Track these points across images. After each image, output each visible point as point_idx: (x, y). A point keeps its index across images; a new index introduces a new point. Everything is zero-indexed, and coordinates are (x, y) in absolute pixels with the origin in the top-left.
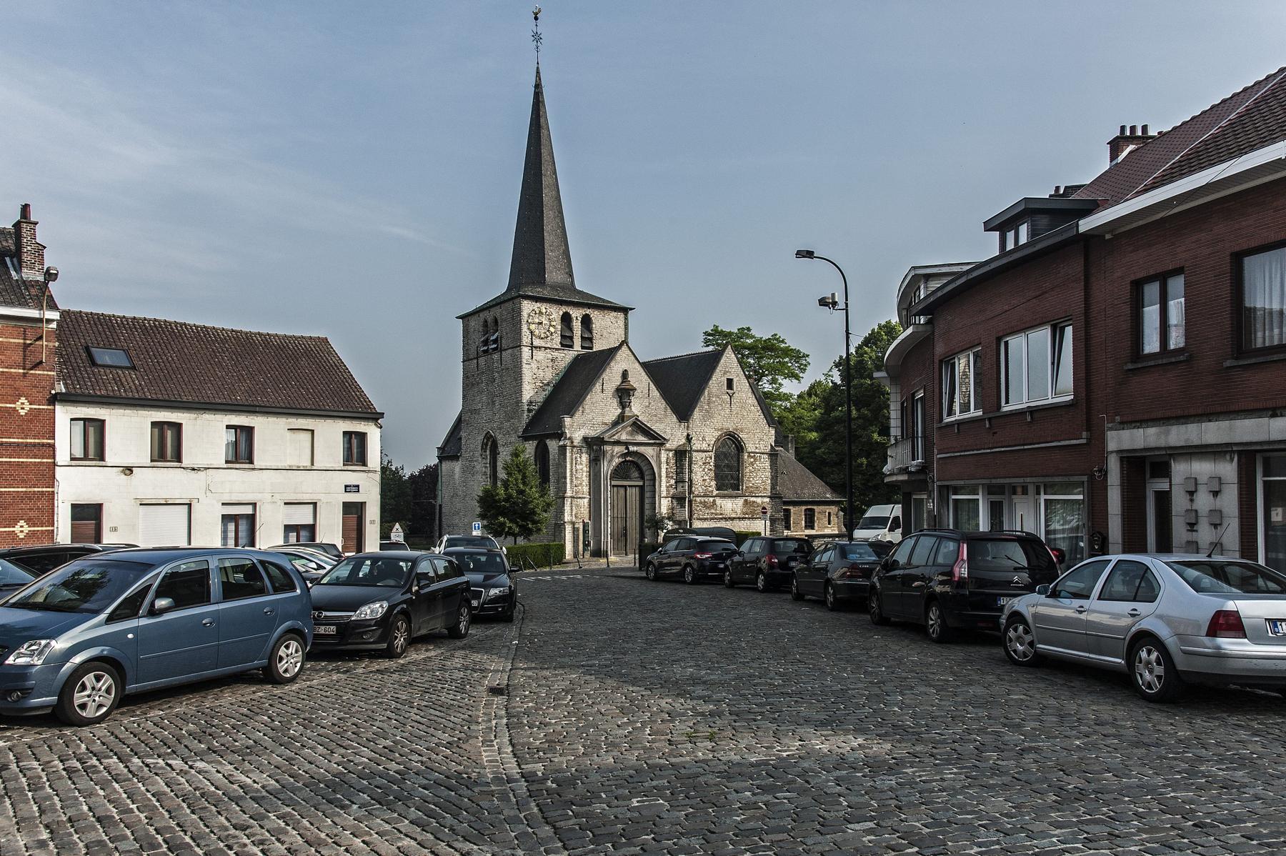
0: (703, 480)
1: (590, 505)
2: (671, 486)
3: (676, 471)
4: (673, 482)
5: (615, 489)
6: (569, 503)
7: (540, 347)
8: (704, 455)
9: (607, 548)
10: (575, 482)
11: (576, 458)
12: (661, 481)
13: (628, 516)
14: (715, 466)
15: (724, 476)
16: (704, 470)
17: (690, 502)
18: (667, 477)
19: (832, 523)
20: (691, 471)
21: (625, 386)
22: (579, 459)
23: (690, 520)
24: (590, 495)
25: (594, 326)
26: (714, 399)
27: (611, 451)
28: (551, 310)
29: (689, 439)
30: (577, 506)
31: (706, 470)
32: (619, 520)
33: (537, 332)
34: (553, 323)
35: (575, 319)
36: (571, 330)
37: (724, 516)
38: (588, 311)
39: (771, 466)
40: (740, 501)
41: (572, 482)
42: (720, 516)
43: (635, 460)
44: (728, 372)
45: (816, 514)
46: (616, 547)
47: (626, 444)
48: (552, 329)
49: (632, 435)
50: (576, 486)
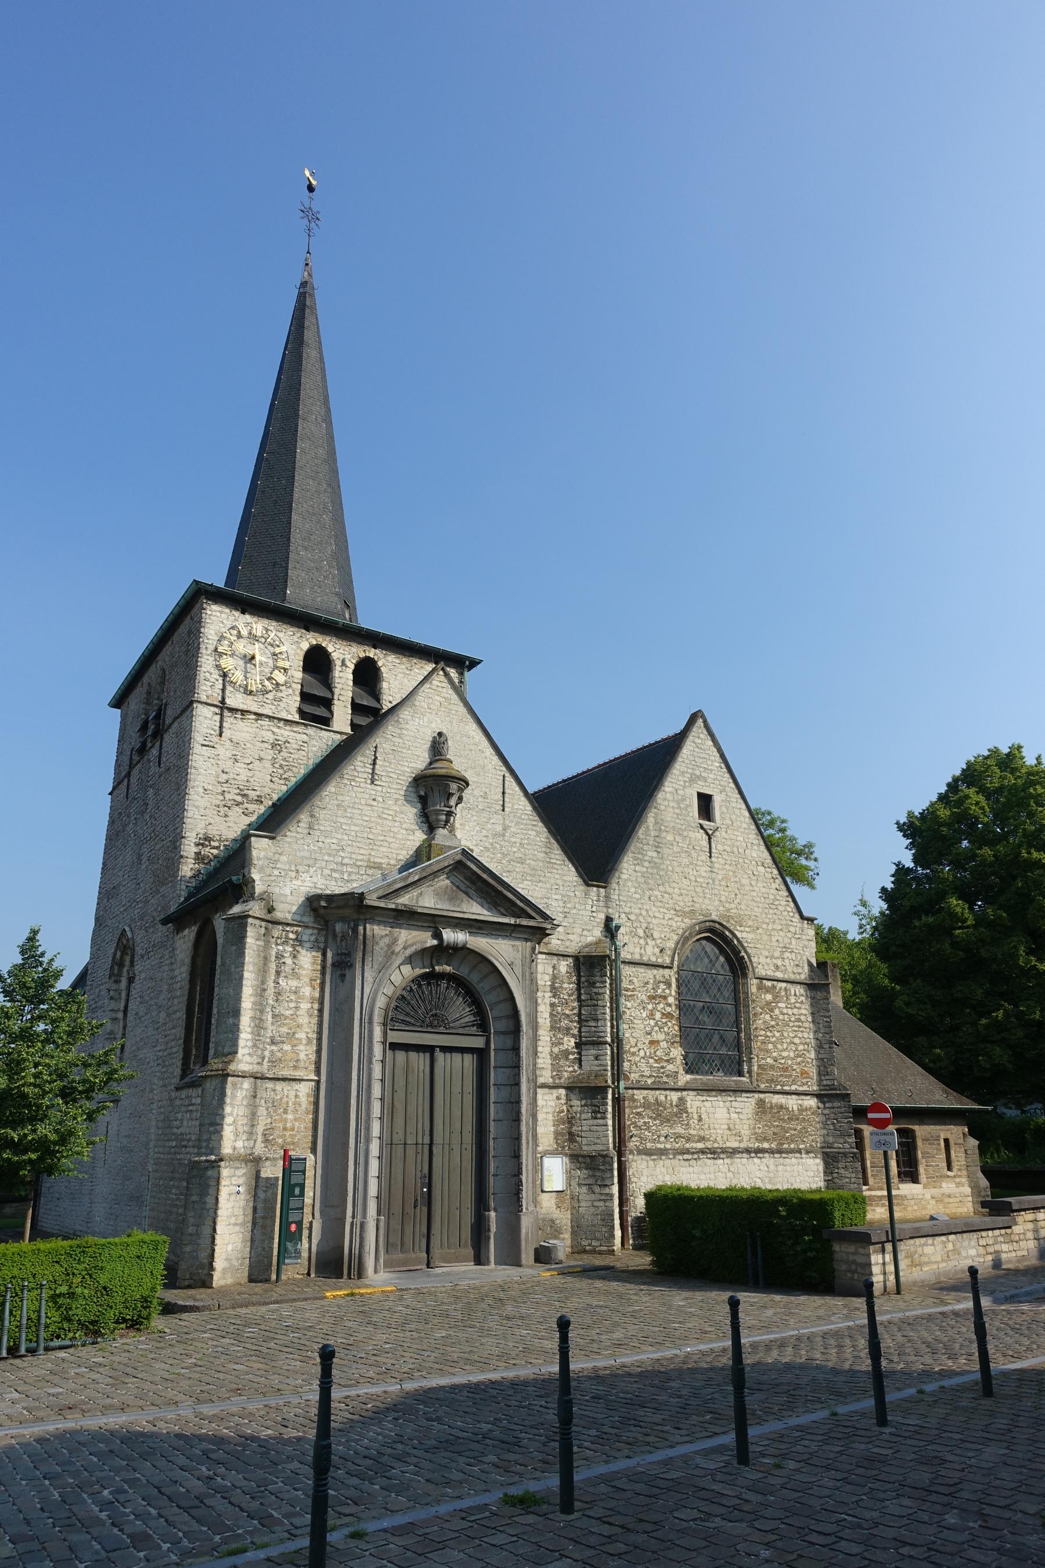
0: (652, 1042)
1: (316, 1104)
2: (566, 1053)
3: (580, 1015)
4: (570, 1043)
5: (401, 1055)
6: (240, 1095)
7: (243, 712)
8: (650, 974)
9: (361, 1246)
10: (270, 1030)
11: (279, 956)
12: (535, 1039)
13: (438, 1139)
14: (679, 1007)
15: (702, 1036)
16: (651, 1016)
17: (618, 1101)
18: (553, 1028)
19: (955, 1165)
20: (617, 1015)
21: (441, 769)
22: (289, 961)
23: (620, 1154)
24: (318, 1071)
25: (385, 685)
26: (670, 837)
27: (387, 940)
28: (280, 635)
29: (610, 930)
30: (274, 1105)
31: (658, 1016)
32: (411, 1151)
33: (238, 676)
34: (280, 664)
35: (338, 663)
36: (328, 685)
37: (709, 1145)
38: (372, 653)
39: (812, 1014)
40: (747, 1104)
41: (259, 1026)
42: (700, 1145)
43: (463, 971)
44: (699, 777)
45: (919, 1143)
46: (396, 1239)
47: (434, 922)
48: (280, 677)
49: (452, 899)
50: (273, 1042)
